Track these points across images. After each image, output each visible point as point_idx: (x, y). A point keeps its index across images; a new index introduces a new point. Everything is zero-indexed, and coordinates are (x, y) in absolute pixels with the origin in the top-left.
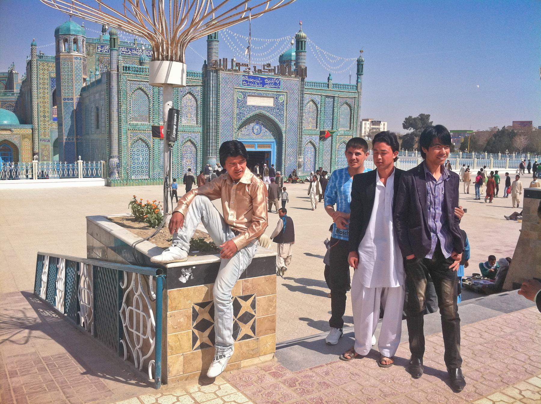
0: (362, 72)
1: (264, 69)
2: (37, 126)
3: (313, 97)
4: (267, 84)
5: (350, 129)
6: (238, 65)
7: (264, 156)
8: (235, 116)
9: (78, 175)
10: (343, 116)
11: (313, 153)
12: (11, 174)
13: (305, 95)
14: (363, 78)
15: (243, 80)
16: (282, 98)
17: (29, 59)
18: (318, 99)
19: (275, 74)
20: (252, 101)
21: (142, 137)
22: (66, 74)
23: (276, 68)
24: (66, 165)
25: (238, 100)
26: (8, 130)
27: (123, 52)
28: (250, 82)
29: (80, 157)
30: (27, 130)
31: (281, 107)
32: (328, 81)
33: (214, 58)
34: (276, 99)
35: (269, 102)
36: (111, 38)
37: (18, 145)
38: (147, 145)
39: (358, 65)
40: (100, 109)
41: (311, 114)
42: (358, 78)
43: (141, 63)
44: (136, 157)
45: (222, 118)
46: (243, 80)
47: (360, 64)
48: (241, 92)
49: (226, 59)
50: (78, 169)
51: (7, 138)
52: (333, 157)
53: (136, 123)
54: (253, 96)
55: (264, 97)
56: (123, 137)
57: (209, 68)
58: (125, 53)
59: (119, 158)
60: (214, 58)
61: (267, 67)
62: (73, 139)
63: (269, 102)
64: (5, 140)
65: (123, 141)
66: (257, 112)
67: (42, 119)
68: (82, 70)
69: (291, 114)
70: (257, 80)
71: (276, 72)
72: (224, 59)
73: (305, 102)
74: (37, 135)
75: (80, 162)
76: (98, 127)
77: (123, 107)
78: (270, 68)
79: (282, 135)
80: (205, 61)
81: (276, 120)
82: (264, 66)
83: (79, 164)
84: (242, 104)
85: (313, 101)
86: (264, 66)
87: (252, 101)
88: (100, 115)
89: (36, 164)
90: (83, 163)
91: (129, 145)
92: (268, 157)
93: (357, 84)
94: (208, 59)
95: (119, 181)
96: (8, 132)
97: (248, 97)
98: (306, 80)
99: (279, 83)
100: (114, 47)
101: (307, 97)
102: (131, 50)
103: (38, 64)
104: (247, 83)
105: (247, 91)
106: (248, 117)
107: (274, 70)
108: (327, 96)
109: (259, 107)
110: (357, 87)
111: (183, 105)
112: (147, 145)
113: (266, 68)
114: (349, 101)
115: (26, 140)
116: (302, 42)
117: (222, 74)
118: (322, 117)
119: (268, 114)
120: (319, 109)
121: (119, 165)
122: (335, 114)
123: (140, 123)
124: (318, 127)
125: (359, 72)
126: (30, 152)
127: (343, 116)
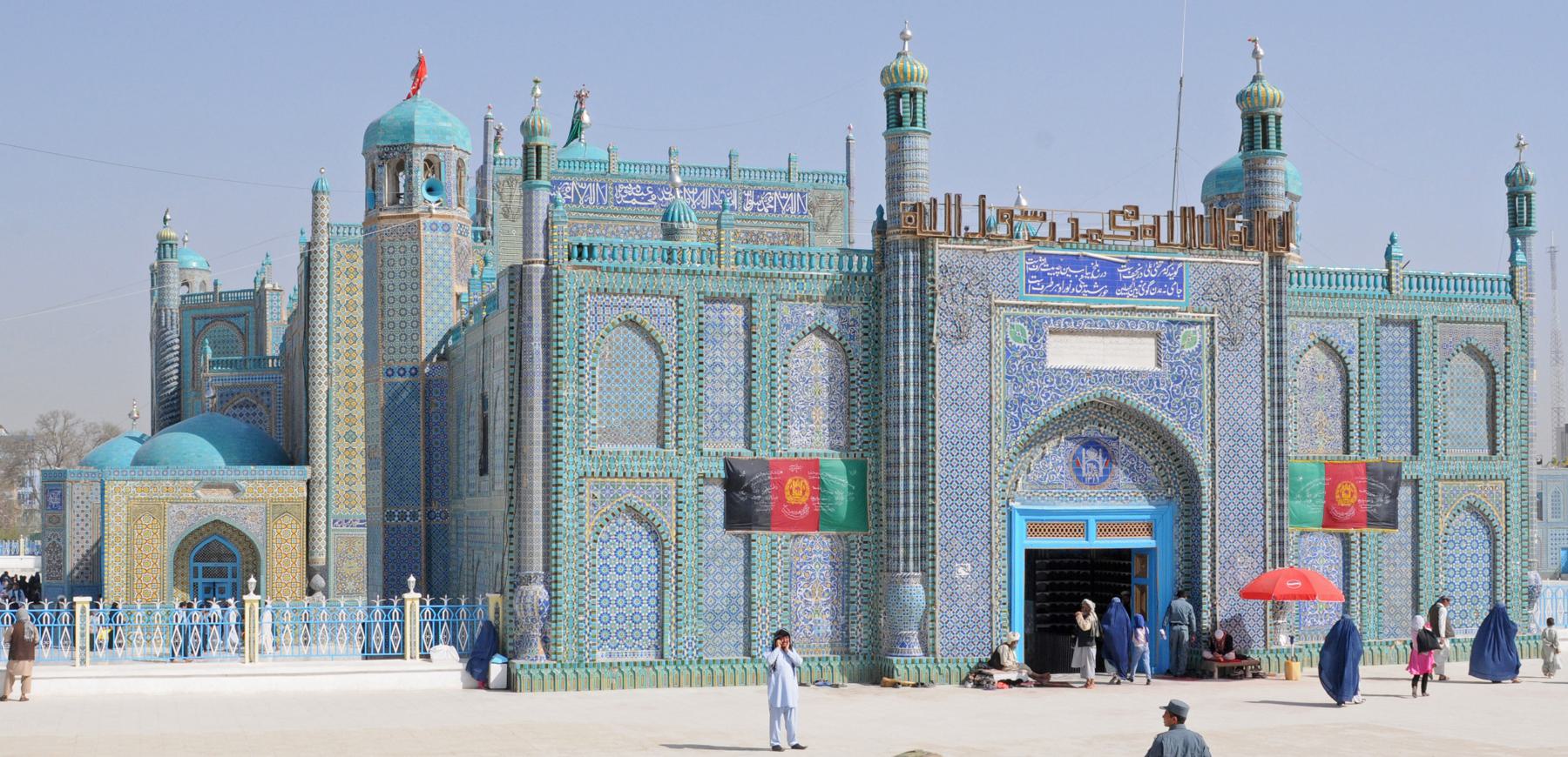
0: (1529, 223)
1: (1113, 225)
2: (323, 470)
3: (1331, 330)
4: (1128, 282)
5: (1494, 452)
6: (1006, 215)
7: (1128, 568)
8: (999, 410)
9: (402, 647)
10: (1459, 402)
11: (649, 577)
12: (369, 637)
13: (1290, 323)
14: (1537, 243)
15: (1029, 275)
16: (1192, 340)
17: (308, 237)
18: (1344, 335)
19: (1158, 243)
20: (1064, 353)
21: (636, 500)
22: (397, 281)
23: (1164, 222)
24: (445, 608)
25: (1010, 350)
26: (225, 486)
27: (629, 198)
28: (1057, 280)
29: (412, 579)
30: (287, 482)
31: (1188, 370)
32: (1388, 266)
33: (912, 197)
34: (1163, 341)
35: (1137, 355)
36: (526, 148)
37: (258, 541)
38: (655, 534)
39: (1512, 196)
40: (491, 402)
41: (1321, 397)
42: (1514, 248)
43: (670, 233)
44: (613, 578)
45: (945, 422)
46: (1029, 275)
47: (1518, 192)
48: (1023, 319)
49: (959, 197)
50: (402, 626)
51: (221, 516)
52: (1427, 567)
53: (614, 448)
54: (1071, 332)
55: (1115, 334)
56: (567, 502)
57: (894, 236)
58: (634, 202)
59: (550, 583)
60: (912, 197)
61: (1126, 217)
62: (414, 516)
63: (1137, 355)
64: (217, 523)
65: (566, 520)
66: (1091, 392)
67: (342, 445)
68: (454, 266)
69: (1241, 399)
70: (1085, 267)
71: (1164, 239)
72: (948, 196)
73: (1291, 350)
74: (323, 503)
75: (412, 597)
76: (484, 470)
77: (568, 392)
78: (1136, 224)
79: (1198, 480)
80: (880, 211)
81: (1171, 423)
82: (1113, 214)
83: (408, 604)
84: (1026, 364)
85: (1325, 344)
86: (1113, 214)
87: (1064, 353)
88: (491, 425)
89: (418, 606)
90: (422, 602)
91: (588, 532)
92: (1143, 574)
93: (1512, 273)
94: (893, 203)
95: (546, 672)
96: (226, 495)
97: (1051, 339)
98: (1295, 260)
99: (1180, 278)
100: (538, 176)
101: (1299, 332)
102: (655, 189)
103: (334, 254)
104: (1046, 281)
105: (1046, 313)
106: (1056, 413)
107: (1155, 230)
108: (1385, 321)
109: (1099, 375)
110: (1512, 283)
111: (794, 377)
112: (655, 534)
113: (1119, 220)
114: (1482, 338)
115: (287, 519)
116: (1265, 119)
117: (943, 253)
118: (1367, 407)
119: (1135, 400)
120: (1354, 376)
121: (551, 613)
122: (1425, 395)
123: (629, 449)
124: (1355, 447)
125: (1519, 222)
126: (300, 563)
127: (1459, 402)
